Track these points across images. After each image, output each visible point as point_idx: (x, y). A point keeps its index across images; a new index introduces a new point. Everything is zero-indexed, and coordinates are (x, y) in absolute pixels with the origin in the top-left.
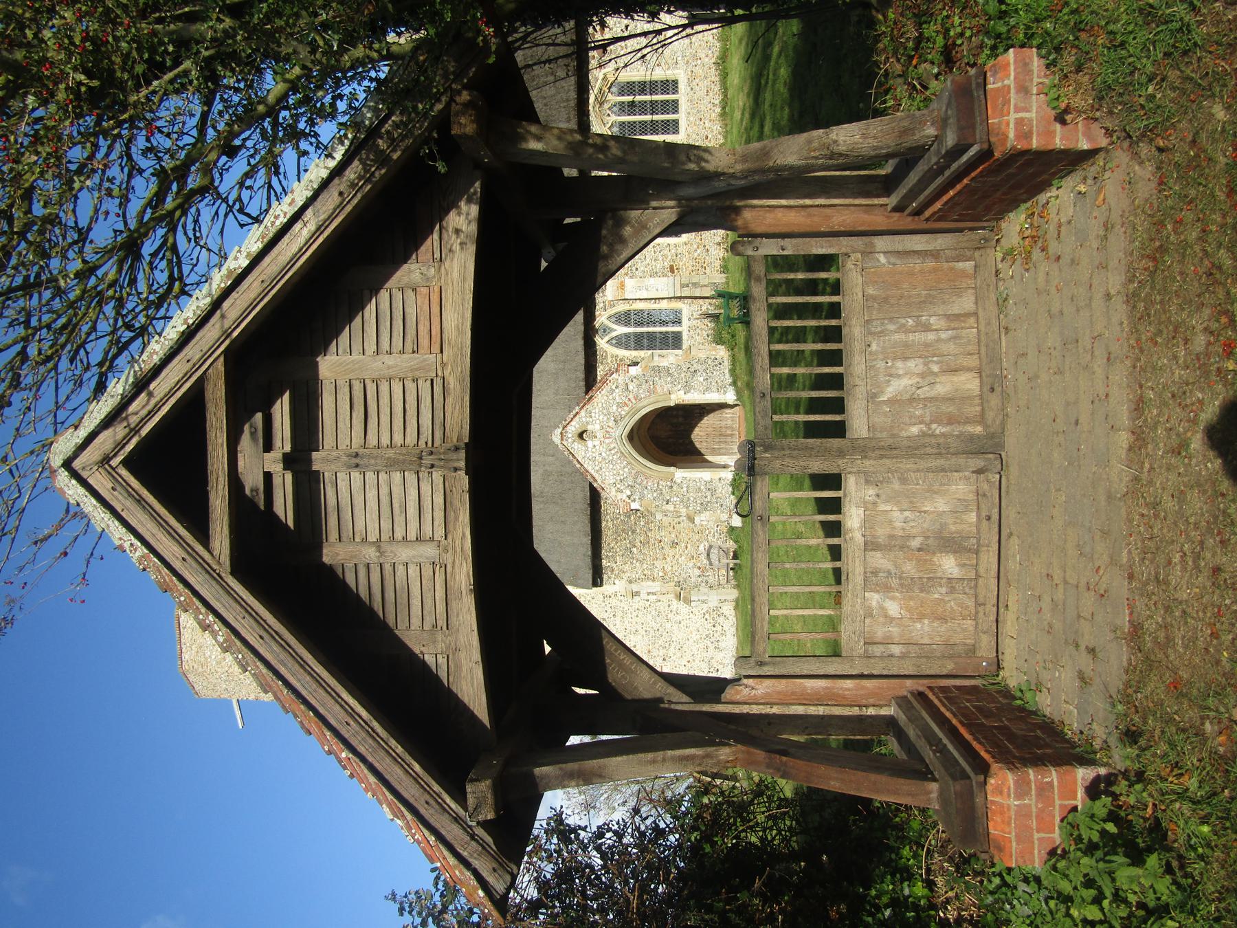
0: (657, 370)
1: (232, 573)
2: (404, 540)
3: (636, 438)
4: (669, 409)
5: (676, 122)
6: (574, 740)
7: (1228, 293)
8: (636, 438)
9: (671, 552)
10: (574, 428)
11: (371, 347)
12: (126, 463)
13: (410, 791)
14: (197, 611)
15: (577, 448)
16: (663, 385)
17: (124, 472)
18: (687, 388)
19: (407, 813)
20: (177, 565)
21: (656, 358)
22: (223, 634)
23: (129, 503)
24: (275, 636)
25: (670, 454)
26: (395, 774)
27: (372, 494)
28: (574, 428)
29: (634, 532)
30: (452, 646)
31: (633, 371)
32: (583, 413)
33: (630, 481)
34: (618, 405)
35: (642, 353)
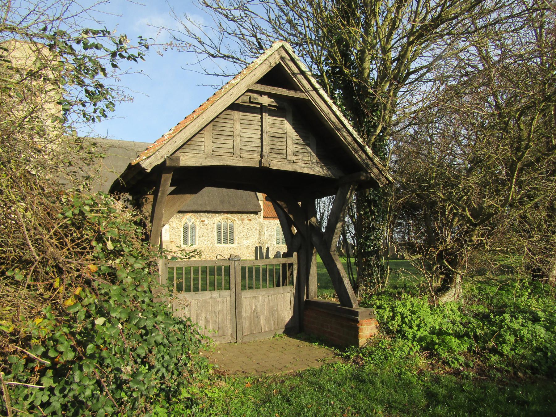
12: (280, 63)
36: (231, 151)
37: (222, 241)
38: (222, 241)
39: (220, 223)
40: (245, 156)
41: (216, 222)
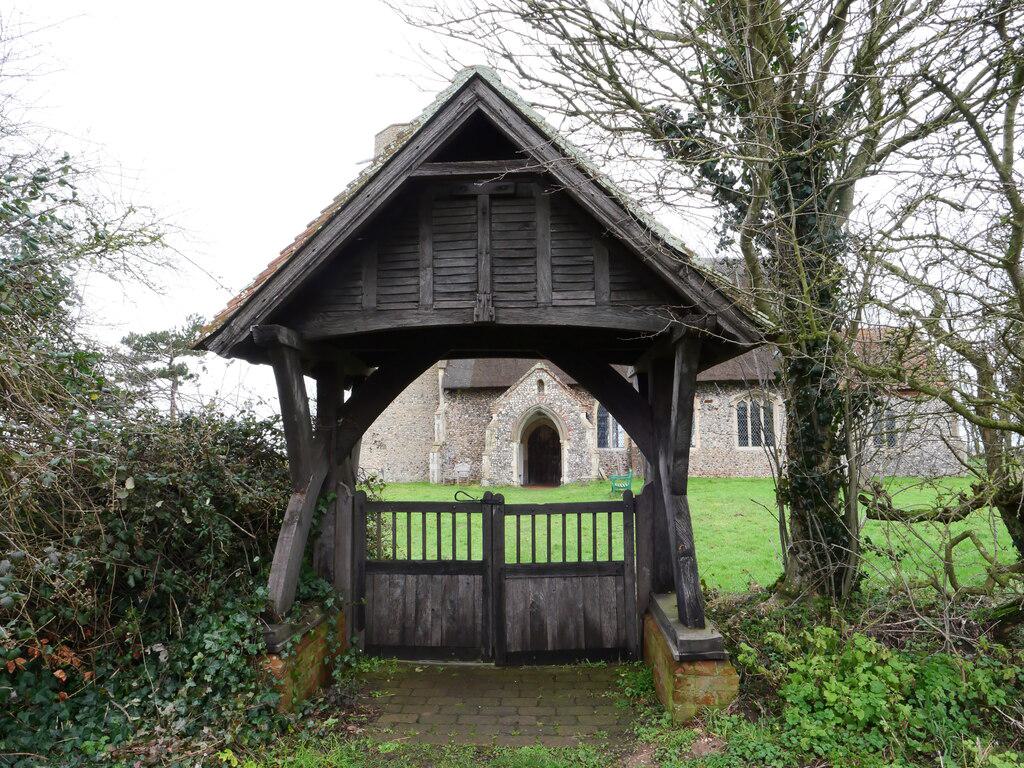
0: (582, 432)
1: (410, 179)
2: (434, 289)
3: (538, 417)
4: (557, 438)
5: (747, 445)
6: (311, 385)
7: (310, 587)
8: (538, 417)
9: (465, 439)
10: (546, 377)
11: (556, 262)
12: (479, 112)
13: (320, 244)
14: (384, 156)
15: (534, 379)
16: (574, 435)
17: (473, 110)
18: (571, 451)
19: (257, 288)
20: (415, 144)
21: (591, 431)
22: (371, 172)
23: (357, 210)
24: (369, 205)
25: (530, 439)
26: (333, 230)
27: (463, 263)
28: (546, 377)
29: (479, 415)
30: (372, 310)
31: (583, 416)
32: (555, 383)
33: (511, 414)
34: (561, 406)
35: (595, 421)
36: (413, 298)
37: (750, 441)
38: (750, 441)
39: (742, 405)
40: (444, 305)
41: (735, 404)
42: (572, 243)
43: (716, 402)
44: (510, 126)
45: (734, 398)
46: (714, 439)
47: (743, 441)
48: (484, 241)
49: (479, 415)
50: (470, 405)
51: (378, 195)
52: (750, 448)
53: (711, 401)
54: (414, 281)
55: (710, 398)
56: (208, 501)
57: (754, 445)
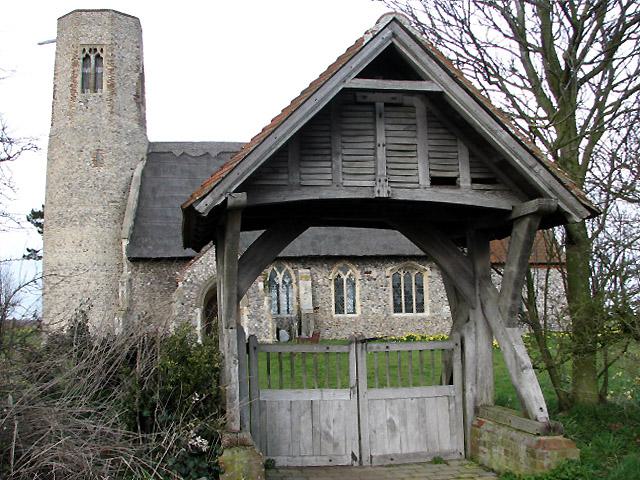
5: (401, 311)
11: (432, 155)
17: (390, 42)
40: (349, 183)
42: (442, 143)
43: (374, 274)
44: (415, 56)
45: (388, 270)
46: (373, 306)
47: (398, 309)
48: (381, 139)
49: (160, 283)
50: (151, 272)
51: (322, 100)
52: (403, 314)
53: (370, 272)
54: (329, 164)
55: (369, 269)
56: (580, 266)
57: (407, 311)
